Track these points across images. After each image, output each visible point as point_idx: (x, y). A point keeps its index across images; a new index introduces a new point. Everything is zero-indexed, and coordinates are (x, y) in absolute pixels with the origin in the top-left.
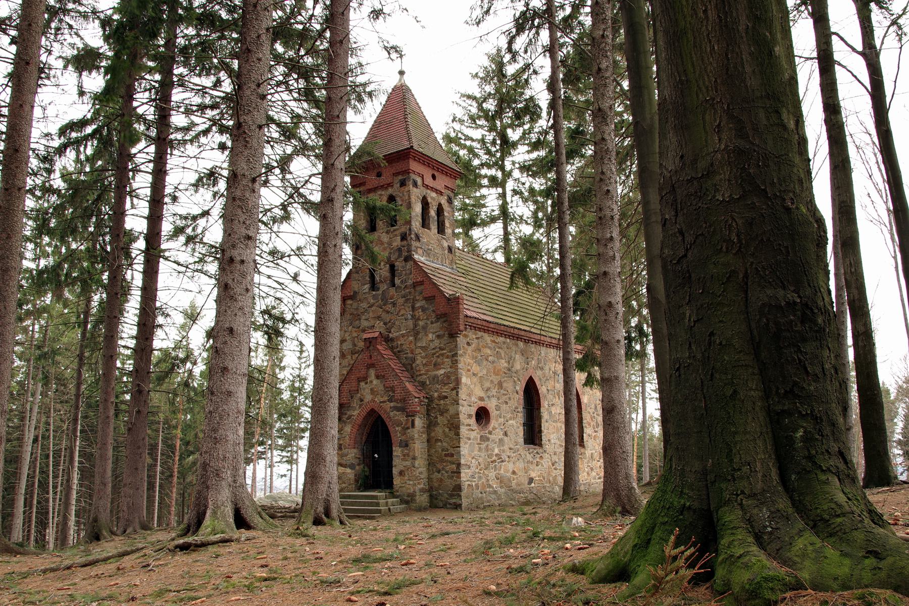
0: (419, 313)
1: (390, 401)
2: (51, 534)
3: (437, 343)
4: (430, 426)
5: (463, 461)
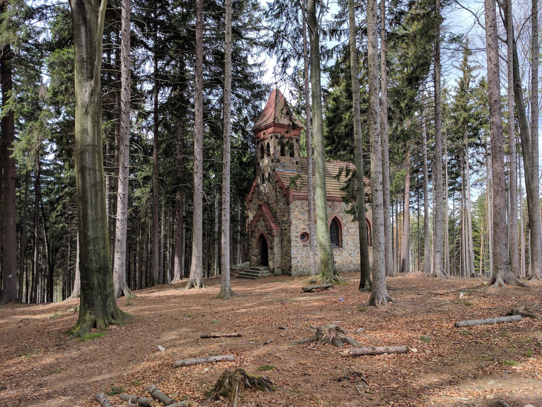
0: (278, 193)
1: (267, 230)
2: (469, 233)
3: (284, 206)
4: (282, 241)
5: (292, 256)
